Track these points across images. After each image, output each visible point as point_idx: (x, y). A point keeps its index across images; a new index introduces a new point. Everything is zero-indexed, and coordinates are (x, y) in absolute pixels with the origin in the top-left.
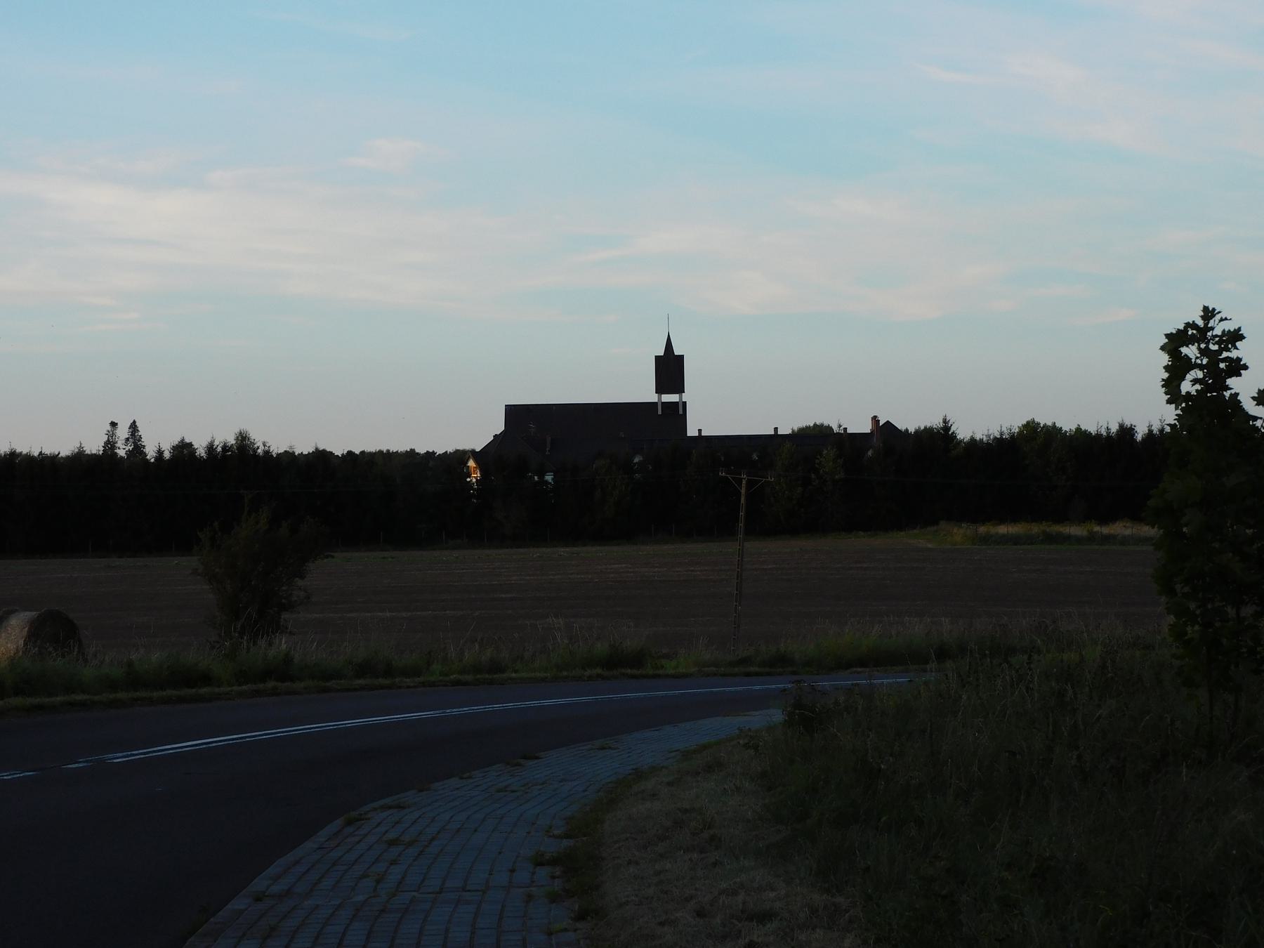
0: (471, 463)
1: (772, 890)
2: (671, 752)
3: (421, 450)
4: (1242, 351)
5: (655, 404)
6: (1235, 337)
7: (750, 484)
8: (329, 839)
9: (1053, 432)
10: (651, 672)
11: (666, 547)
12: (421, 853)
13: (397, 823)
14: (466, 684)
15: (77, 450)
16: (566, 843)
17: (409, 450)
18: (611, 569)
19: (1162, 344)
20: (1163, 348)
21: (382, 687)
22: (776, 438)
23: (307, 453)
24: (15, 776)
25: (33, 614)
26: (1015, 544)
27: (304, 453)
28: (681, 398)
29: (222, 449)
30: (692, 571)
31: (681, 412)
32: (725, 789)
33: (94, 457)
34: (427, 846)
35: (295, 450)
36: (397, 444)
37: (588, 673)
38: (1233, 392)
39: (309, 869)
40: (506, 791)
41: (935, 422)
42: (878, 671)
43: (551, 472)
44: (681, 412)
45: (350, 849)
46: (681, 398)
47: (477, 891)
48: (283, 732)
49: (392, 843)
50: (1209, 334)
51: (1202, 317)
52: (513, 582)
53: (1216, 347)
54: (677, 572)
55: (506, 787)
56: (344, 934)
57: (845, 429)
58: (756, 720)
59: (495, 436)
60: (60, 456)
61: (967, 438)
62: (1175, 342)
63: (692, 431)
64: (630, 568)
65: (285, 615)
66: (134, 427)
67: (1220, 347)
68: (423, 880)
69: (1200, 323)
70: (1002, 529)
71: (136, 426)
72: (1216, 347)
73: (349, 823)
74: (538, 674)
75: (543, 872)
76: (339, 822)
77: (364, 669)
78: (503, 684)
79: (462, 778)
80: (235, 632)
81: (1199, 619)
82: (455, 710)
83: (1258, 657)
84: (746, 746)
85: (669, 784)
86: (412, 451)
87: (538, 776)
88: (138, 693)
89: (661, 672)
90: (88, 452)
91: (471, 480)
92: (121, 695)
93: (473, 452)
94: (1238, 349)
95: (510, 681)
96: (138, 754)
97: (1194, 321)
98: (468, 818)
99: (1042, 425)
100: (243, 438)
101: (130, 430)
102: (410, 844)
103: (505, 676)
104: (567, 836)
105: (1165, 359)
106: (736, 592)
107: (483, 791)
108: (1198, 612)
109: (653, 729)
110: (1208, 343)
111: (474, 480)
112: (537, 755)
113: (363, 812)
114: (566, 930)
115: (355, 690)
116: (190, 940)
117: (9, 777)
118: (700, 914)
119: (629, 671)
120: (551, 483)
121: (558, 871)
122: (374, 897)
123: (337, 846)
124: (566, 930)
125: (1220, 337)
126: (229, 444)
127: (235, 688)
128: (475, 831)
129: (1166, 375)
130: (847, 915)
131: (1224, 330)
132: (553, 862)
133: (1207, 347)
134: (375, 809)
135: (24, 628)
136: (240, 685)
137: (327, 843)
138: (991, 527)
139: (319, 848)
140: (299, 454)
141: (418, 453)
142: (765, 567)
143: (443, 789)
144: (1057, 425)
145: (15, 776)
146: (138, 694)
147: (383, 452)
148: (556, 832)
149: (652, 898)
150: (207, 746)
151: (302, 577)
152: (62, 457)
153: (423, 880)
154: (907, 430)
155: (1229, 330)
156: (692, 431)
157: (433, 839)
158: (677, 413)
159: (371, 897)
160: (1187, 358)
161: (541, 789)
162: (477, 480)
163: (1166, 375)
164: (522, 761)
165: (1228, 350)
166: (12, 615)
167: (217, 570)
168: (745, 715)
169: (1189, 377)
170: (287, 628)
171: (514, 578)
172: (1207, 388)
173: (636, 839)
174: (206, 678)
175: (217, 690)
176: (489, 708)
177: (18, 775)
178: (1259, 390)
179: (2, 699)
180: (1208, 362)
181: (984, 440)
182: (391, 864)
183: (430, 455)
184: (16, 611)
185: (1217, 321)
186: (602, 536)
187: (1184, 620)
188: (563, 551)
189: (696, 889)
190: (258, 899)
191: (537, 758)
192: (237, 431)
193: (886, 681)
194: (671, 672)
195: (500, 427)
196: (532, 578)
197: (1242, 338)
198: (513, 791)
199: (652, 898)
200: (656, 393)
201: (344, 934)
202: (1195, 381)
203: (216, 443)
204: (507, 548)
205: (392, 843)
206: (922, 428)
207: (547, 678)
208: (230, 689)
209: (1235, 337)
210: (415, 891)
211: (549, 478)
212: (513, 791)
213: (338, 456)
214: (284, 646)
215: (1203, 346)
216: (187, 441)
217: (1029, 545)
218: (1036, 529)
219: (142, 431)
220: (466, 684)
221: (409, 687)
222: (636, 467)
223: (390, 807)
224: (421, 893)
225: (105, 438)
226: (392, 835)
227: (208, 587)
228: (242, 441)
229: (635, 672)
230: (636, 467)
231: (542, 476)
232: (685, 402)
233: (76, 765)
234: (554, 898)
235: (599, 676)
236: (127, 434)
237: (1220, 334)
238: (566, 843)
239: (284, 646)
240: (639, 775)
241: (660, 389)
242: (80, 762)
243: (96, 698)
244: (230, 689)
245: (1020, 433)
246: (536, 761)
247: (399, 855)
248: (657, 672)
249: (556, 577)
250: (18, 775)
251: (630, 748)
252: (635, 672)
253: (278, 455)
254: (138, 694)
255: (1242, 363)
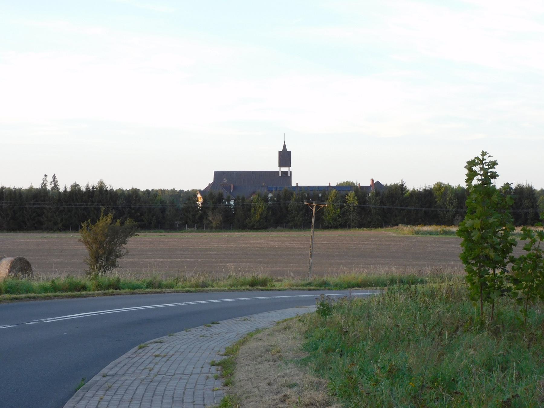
0: (199, 196)
1: (298, 376)
2: (272, 322)
3: (178, 189)
4: (497, 169)
5: (278, 172)
6: (494, 164)
7: (317, 207)
8: (132, 354)
9: (448, 188)
10: (269, 288)
11: (281, 233)
12: (167, 360)
13: (159, 348)
14: (192, 292)
15: (30, 186)
16: (224, 357)
17: (172, 189)
18: (258, 242)
19: (465, 166)
20: (465, 167)
21: (157, 293)
22: (329, 188)
23: (129, 189)
24: (7, 327)
25: (11, 259)
26: (430, 235)
27: (127, 190)
28: (289, 169)
29: (92, 187)
30: (292, 244)
31: (289, 175)
32: (289, 337)
33: (37, 189)
34: (170, 358)
35: (123, 188)
36: (168, 186)
37: (243, 288)
38: (493, 185)
39: (124, 366)
40: (204, 337)
41: (399, 182)
42: (365, 289)
43: (233, 200)
44: (289, 175)
45: (140, 358)
46: (289, 169)
47: (188, 375)
48: (115, 311)
49: (157, 356)
50: (484, 162)
51: (481, 155)
52: (215, 247)
53: (487, 167)
54: (286, 244)
55: (204, 335)
56: (136, 390)
57: (359, 184)
58: (302, 310)
59: (210, 184)
60: (22, 189)
61: (411, 190)
62: (471, 164)
63: (294, 184)
64: (266, 242)
65: (118, 260)
66: (54, 177)
67: (488, 167)
68: (168, 370)
69: (481, 158)
70: (425, 228)
71: (55, 176)
72: (487, 167)
73: (140, 348)
74: (222, 288)
75: (214, 369)
76: (137, 348)
77: (150, 285)
78: (207, 292)
79: (187, 331)
80: (96, 268)
81: (478, 274)
82: (186, 303)
83: (502, 289)
84: (299, 320)
85: (268, 335)
86: (174, 189)
87: (217, 331)
88: (56, 294)
89: (273, 288)
90: (34, 187)
91: (199, 203)
92: (49, 294)
93: (200, 191)
94: (495, 168)
95: (210, 291)
96: (57, 319)
97: (478, 157)
98: (187, 347)
99: (443, 184)
100: (101, 183)
101: (53, 178)
102: (164, 356)
103: (208, 289)
104: (225, 355)
105: (466, 171)
106: (310, 253)
107: (195, 336)
108: (477, 271)
109: (266, 312)
110: (483, 165)
111: (200, 203)
112: (218, 322)
113: (146, 344)
114: (220, 390)
115: (146, 293)
116: (78, 391)
117: (5, 327)
118: (269, 384)
119: (260, 288)
120: (232, 205)
121: (219, 368)
122: (149, 376)
123: (135, 357)
124: (220, 390)
125: (489, 163)
126: (95, 186)
127: (96, 292)
128: (190, 352)
129: (467, 178)
130: (324, 386)
131: (490, 161)
132: (218, 365)
133: (483, 167)
134: (151, 343)
135: (8, 264)
136: (98, 291)
137: (132, 356)
138: (421, 227)
139: (128, 358)
140: (125, 190)
141: (176, 190)
142: (323, 243)
143: (179, 335)
144: (450, 184)
145: (7, 327)
146: (56, 294)
147: (161, 190)
148: (221, 353)
149: (252, 378)
150: (85, 316)
151: (125, 244)
152: (23, 189)
153: (168, 370)
154: (387, 185)
155: (492, 161)
156: (294, 184)
157: (173, 355)
158: (287, 176)
159: (147, 376)
160: (475, 172)
161: (218, 336)
162: (201, 203)
163: (467, 178)
164: (211, 325)
165: (491, 168)
166: (3, 259)
167: (89, 240)
168: (305, 307)
169: (476, 178)
170: (119, 265)
171: (216, 245)
172: (483, 183)
173: (250, 356)
174: (84, 288)
175: (88, 293)
176: (200, 302)
177: (8, 327)
178: (504, 184)
179: (1, 295)
180: (483, 173)
181: (418, 190)
182: (156, 364)
183: (181, 191)
184: (5, 257)
185: (487, 157)
186: (253, 228)
187: (472, 274)
188: (237, 234)
189: (269, 375)
190: (104, 376)
191: (218, 323)
192: (99, 180)
193: (359, 294)
194: (278, 288)
195: (211, 180)
196: (224, 245)
197: (497, 164)
198: (206, 337)
199: (252, 378)
200: (279, 166)
201: (136, 390)
202: (478, 180)
203: (90, 185)
204: (214, 232)
205: (157, 356)
206: (393, 184)
207: (225, 290)
208: (94, 292)
209: (494, 164)
210: (164, 374)
211: (232, 202)
212: (206, 337)
213: (142, 191)
214: (117, 275)
215: (481, 166)
216: (77, 183)
217: (436, 235)
218: (439, 228)
219: (58, 179)
220: (192, 292)
221: (168, 293)
222: (269, 198)
223: (157, 342)
224: (167, 375)
225: (42, 182)
226: (156, 354)
227: (85, 247)
228: (101, 184)
229: (262, 288)
230: (269, 198)
231: (229, 201)
232: (291, 171)
233: (32, 323)
234: (217, 378)
235: (247, 289)
236: (51, 180)
237: (488, 162)
238: (224, 357)
239: (117, 275)
240: (257, 331)
241: (281, 165)
242: (33, 322)
243: (40, 295)
244: (94, 292)
245: (434, 187)
246: (218, 325)
247: (159, 361)
248: (271, 288)
249: (234, 245)
250: (8, 327)
251: (256, 320)
252: (262, 288)
253: (116, 190)
254: (56, 294)
255: (497, 174)
